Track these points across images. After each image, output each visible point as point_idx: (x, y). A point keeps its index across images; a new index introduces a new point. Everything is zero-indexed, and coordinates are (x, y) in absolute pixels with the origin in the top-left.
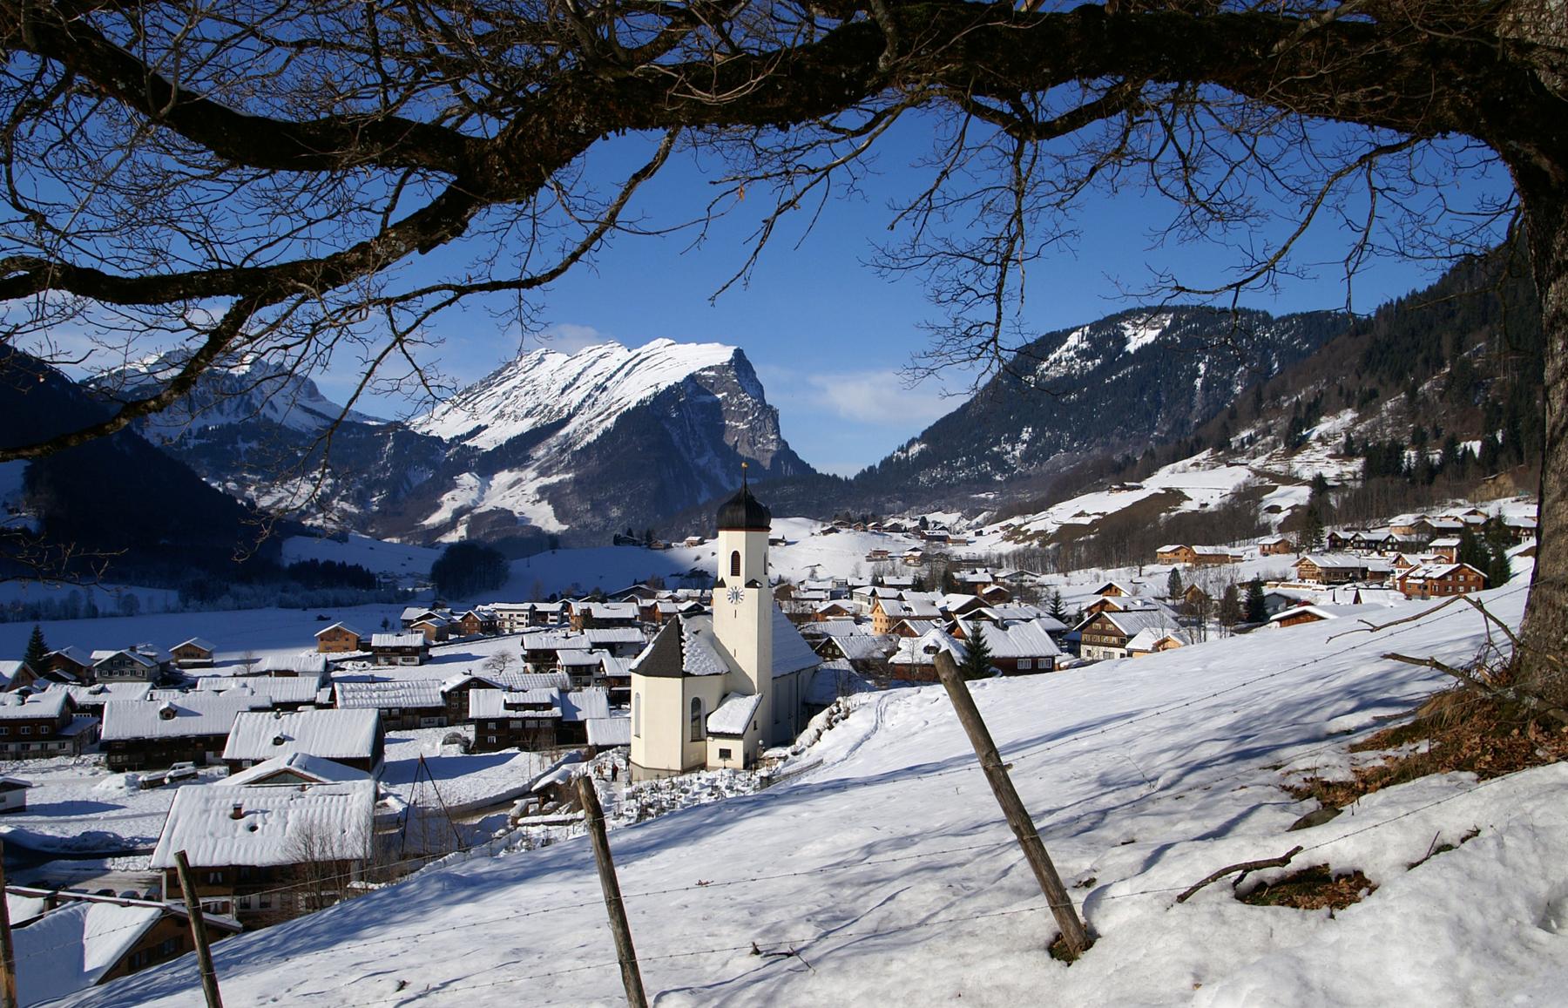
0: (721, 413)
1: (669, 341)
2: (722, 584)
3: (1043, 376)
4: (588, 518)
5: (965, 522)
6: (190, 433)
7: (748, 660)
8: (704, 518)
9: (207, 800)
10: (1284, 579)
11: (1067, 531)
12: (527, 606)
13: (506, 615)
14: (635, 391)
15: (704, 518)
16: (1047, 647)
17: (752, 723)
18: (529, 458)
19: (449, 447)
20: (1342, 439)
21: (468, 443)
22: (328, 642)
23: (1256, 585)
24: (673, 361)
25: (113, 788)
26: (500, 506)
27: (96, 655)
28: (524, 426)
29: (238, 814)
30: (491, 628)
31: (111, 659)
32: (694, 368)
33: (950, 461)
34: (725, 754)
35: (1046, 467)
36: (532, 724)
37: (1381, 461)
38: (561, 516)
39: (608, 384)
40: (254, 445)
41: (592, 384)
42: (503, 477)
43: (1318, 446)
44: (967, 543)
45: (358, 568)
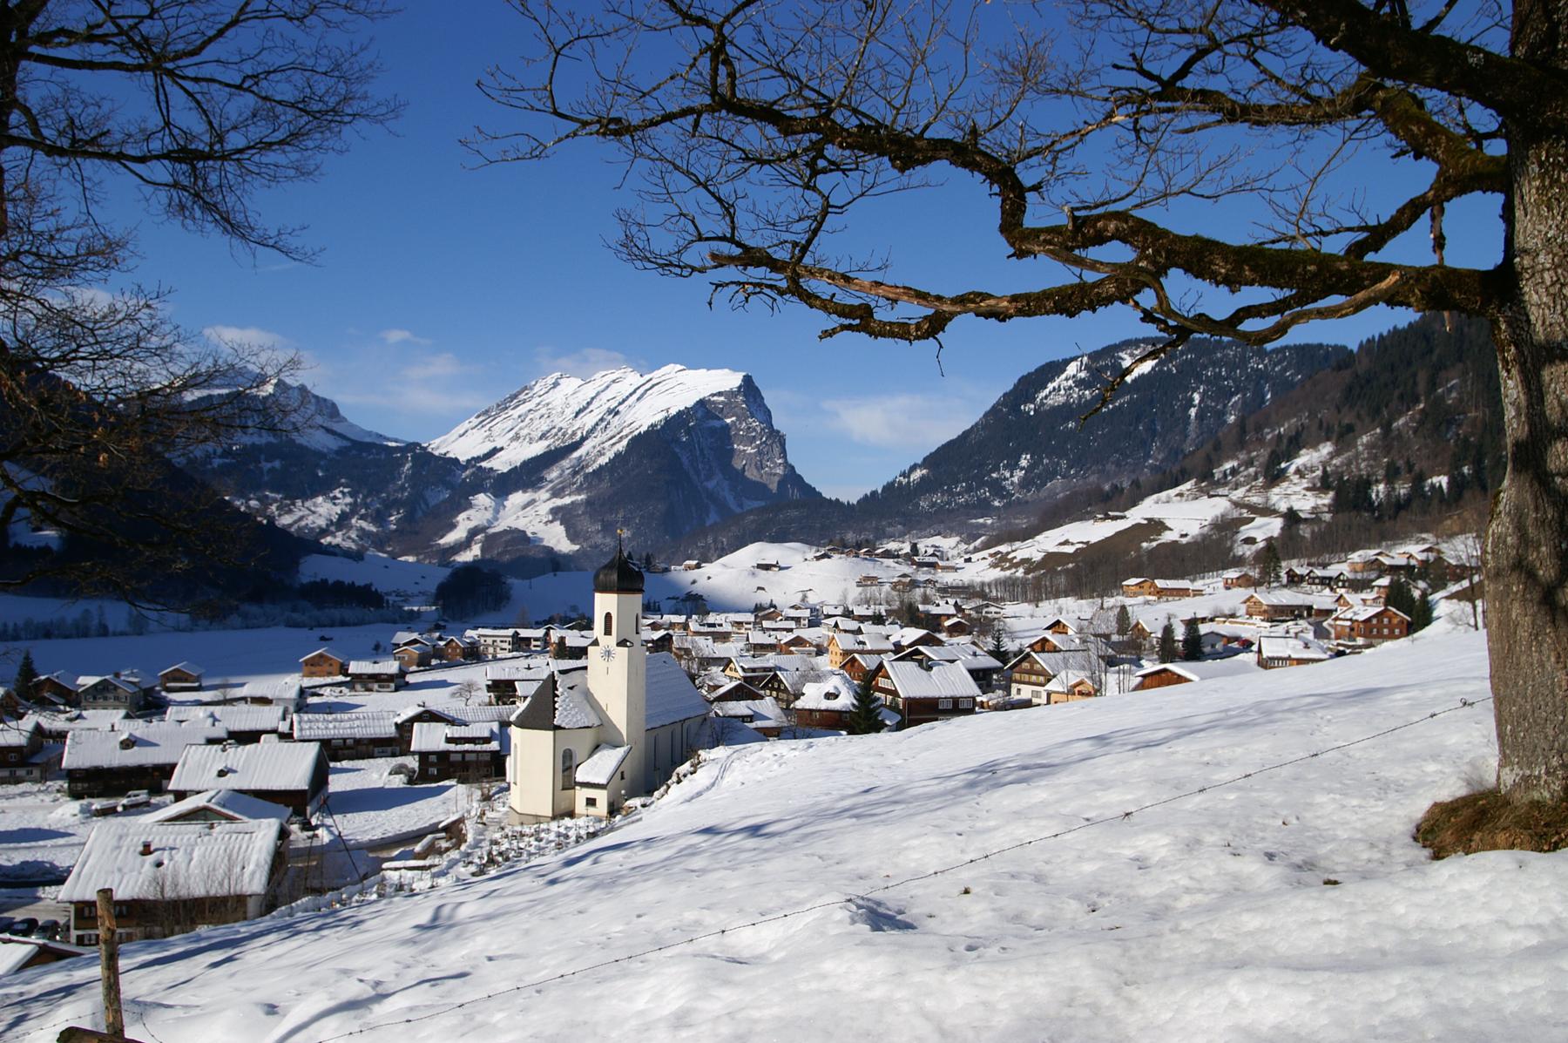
0: (729, 437)
1: (680, 367)
3: (1042, 404)
4: (599, 539)
5: (963, 546)
8: (710, 540)
9: (121, 837)
10: (1233, 616)
11: (1051, 559)
12: (511, 632)
13: (490, 641)
14: (646, 415)
15: (710, 540)
16: (969, 688)
17: (619, 773)
18: (542, 479)
19: (465, 468)
20: (1319, 473)
21: (484, 464)
22: (313, 667)
23: (1192, 624)
25: (67, 816)
26: (514, 526)
27: (82, 680)
28: (538, 448)
29: (147, 850)
30: (474, 654)
31: (95, 686)
33: (954, 483)
35: (1043, 493)
36: (472, 757)
37: (1349, 494)
38: (572, 536)
39: (621, 408)
40: (277, 464)
41: (605, 408)
42: (517, 498)
43: (1295, 478)
44: (956, 569)
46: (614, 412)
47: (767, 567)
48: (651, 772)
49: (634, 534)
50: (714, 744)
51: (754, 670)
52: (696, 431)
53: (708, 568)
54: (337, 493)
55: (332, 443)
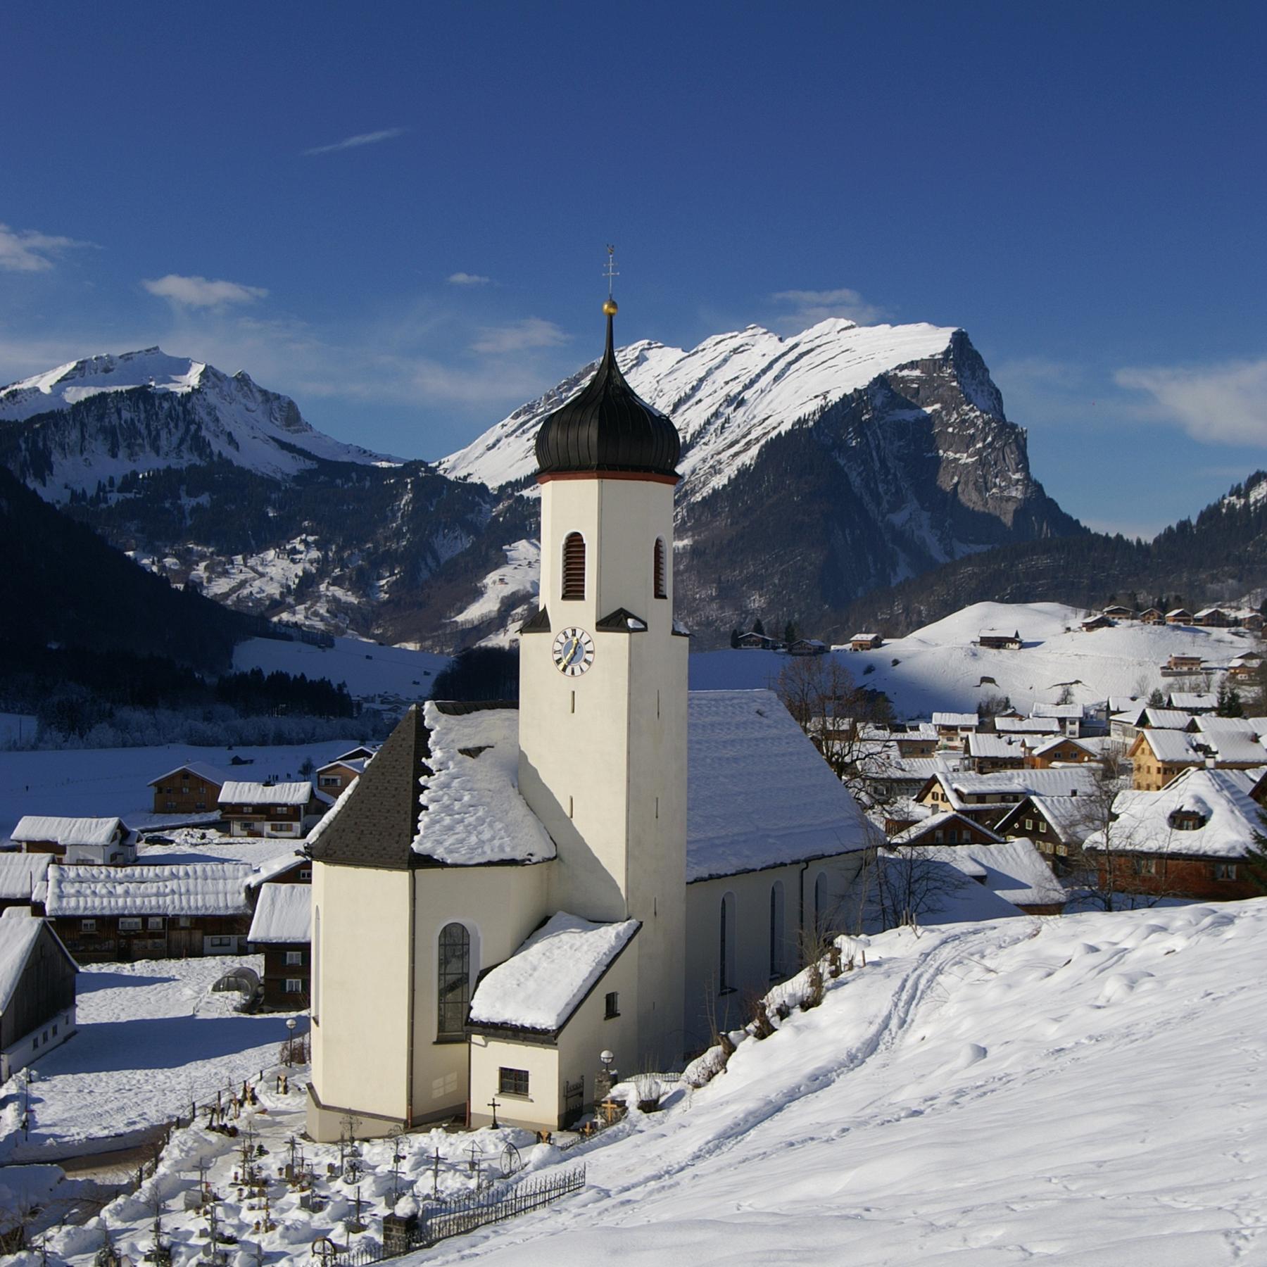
1: (844, 323)
4: (713, 611)
6: (111, 481)
7: (603, 829)
8: (898, 609)
14: (789, 404)
15: (898, 609)
19: (497, 499)
24: (853, 352)
32: (885, 364)
34: (514, 1082)
39: (747, 395)
40: (204, 499)
41: (721, 395)
45: (324, 685)
46: (737, 402)
47: (998, 643)
48: (707, 984)
49: (770, 603)
50: (886, 918)
51: (981, 797)
52: (876, 422)
53: (894, 647)
54: (297, 543)
55: (289, 465)
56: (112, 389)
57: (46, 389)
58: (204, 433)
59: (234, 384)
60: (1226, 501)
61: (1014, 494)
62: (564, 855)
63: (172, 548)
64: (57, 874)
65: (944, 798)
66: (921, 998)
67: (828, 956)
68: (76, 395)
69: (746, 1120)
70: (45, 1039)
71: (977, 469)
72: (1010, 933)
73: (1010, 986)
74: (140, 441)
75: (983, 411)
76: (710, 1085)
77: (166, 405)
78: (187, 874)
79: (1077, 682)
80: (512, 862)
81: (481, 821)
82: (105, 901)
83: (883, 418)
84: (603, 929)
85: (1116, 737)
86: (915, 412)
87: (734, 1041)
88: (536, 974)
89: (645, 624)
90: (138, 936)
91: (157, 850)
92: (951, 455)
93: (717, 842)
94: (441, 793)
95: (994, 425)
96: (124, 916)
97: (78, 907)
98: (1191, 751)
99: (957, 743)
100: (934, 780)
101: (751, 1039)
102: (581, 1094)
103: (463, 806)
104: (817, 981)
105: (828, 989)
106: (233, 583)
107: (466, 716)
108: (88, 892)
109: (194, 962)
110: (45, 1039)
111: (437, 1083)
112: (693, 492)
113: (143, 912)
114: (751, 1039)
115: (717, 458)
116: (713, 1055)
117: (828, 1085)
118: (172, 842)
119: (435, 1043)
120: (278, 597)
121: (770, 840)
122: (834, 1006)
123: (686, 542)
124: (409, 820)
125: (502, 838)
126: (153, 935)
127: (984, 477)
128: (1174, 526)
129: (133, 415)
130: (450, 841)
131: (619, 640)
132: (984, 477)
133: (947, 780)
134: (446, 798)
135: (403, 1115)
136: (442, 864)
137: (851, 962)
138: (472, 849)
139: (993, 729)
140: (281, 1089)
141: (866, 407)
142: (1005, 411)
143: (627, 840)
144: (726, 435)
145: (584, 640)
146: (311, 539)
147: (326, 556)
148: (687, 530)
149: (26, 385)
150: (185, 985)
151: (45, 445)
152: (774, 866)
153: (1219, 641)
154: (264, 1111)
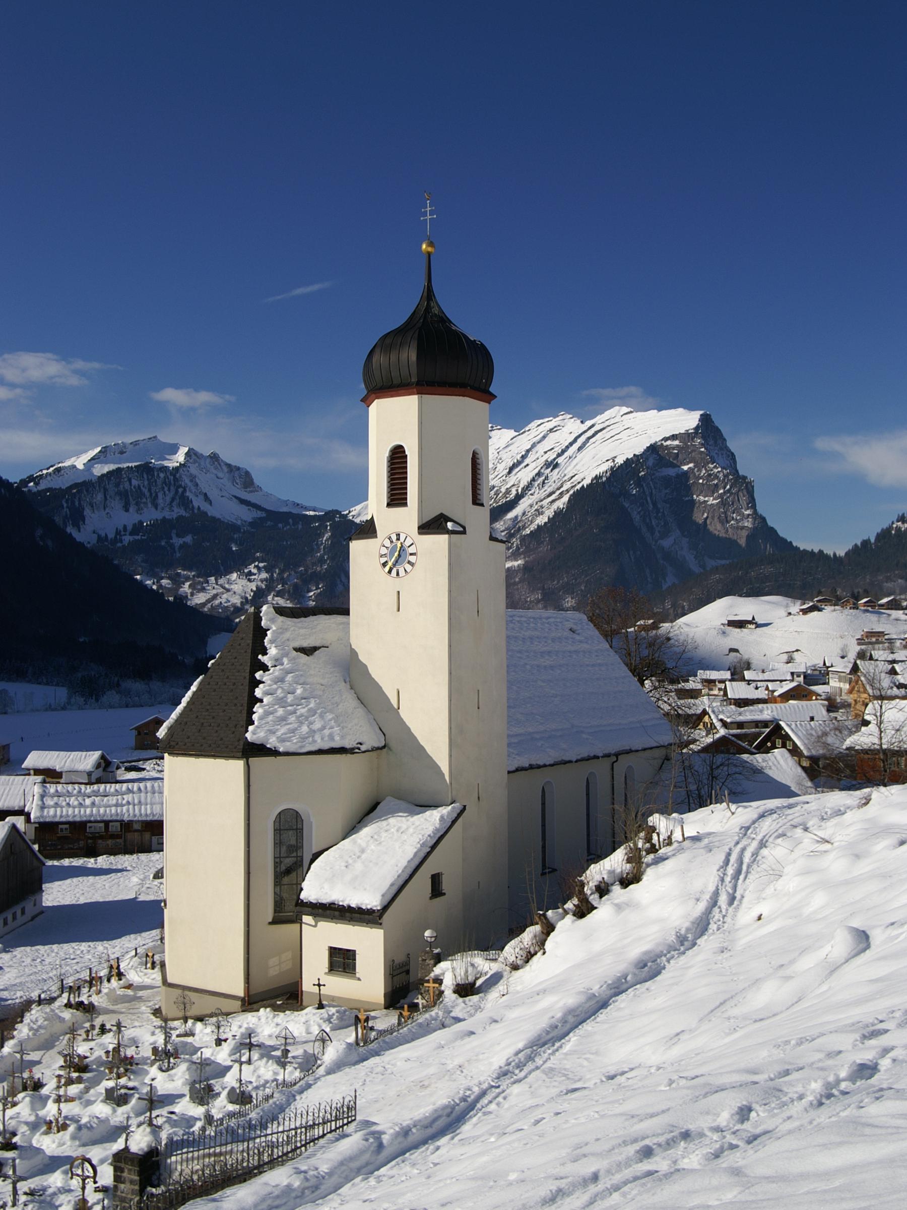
1: (625, 409)
2: (368, 530)
6: (125, 527)
7: (427, 717)
8: (668, 605)
14: (588, 466)
15: (668, 605)
17: (424, 875)
24: (633, 429)
32: (655, 437)
39: (560, 460)
40: (188, 539)
41: (542, 461)
46: (553, 465)
47: (740, 624)
48: (528, 865)
50: (696, 799)
51: (740, 725)
54: (252, 568)
55: (246, 515)
56: (125, 465)
57: (80, 466)
58: (188, 494)
59: (208, 460)
60: (894, 526)
61: (746, 525)
62: (392, 744)
63: (166, 572)
64: (41, 791)
65: (713, 726)
66: (747, 872)
67: (642, 834)
68: (100, 470)
69: (564, 1021)
70: (14, 918)
71: (719, 508)
72: (829, 805)
73: (857, 856)
74: (144, 500)
75: (723, 468)
76: (528, 967)
77: (162, 475)
78: (139, 789)
79: (797, 650)
80: (342, 750)
81: (313, 712)
82: (77, 810)
83: (654, 474)
84: (428, 813)
85: (834, 683)
86: (676, 470)
87: (552, 921)
88: (363, 856)
89: (464, 528)
90: (101, 837)
91: (133, 775)
92: (702, 498)
93: (538, 736)
94: (275, 686)
95: (731, 477)
96: (90, 822)
97: (55, 815)
98: (895, 689)
99: (716, 692)
100: (705, 713)
101: (569, 918)
102: (408, 972)
103: (296, 698)
104: (634, 858)
105: (648, 865)
106: (208, 596)
107: (303, 619)
108: (64, 804)
109: (143, 857)
110: (14, 918)
111: (273, 961)
112: (524, 527)
113: (105, 818)
114: (569, 918)
115: (540, 504)
116: (531, 935)
117: (658, 973)
118: (144, 769)
119: (270, 923)
120: (239, 605)
121: (584, 736)
122: (655, 881)
123: (519, 562)
124: (245, 712)
125: (332, 728)
126: (113, 836)
127: (725, 513)
128: (859, 544)
129: (140, 482)
130: (282, 731)
131: (441, 541)
132: (725, 513)
133: (713, 712)
134: (279, 691)
135: (240, 991)
136: (274, 753)
137: (669, 837)
138: (303, 739)
139: (743, 679)
140: (149, 965)
141: (642, 466)
142: (738, 468)
143: (450, 728)
144: (545, 488)
145: (407, 543)
146: (261, 565)
147: (272, 576)
148: (520, 554)
149: (67, 463)
150: (134, 874)
151: (80, 504)
152: (588, 759)
153: (897, 620)
154: (129, 986)
